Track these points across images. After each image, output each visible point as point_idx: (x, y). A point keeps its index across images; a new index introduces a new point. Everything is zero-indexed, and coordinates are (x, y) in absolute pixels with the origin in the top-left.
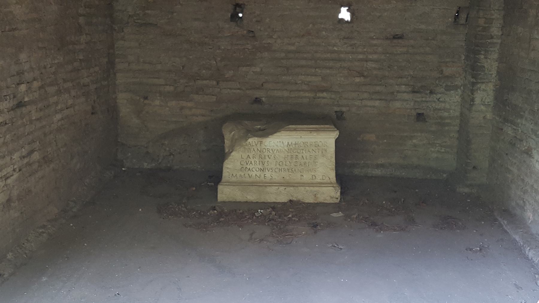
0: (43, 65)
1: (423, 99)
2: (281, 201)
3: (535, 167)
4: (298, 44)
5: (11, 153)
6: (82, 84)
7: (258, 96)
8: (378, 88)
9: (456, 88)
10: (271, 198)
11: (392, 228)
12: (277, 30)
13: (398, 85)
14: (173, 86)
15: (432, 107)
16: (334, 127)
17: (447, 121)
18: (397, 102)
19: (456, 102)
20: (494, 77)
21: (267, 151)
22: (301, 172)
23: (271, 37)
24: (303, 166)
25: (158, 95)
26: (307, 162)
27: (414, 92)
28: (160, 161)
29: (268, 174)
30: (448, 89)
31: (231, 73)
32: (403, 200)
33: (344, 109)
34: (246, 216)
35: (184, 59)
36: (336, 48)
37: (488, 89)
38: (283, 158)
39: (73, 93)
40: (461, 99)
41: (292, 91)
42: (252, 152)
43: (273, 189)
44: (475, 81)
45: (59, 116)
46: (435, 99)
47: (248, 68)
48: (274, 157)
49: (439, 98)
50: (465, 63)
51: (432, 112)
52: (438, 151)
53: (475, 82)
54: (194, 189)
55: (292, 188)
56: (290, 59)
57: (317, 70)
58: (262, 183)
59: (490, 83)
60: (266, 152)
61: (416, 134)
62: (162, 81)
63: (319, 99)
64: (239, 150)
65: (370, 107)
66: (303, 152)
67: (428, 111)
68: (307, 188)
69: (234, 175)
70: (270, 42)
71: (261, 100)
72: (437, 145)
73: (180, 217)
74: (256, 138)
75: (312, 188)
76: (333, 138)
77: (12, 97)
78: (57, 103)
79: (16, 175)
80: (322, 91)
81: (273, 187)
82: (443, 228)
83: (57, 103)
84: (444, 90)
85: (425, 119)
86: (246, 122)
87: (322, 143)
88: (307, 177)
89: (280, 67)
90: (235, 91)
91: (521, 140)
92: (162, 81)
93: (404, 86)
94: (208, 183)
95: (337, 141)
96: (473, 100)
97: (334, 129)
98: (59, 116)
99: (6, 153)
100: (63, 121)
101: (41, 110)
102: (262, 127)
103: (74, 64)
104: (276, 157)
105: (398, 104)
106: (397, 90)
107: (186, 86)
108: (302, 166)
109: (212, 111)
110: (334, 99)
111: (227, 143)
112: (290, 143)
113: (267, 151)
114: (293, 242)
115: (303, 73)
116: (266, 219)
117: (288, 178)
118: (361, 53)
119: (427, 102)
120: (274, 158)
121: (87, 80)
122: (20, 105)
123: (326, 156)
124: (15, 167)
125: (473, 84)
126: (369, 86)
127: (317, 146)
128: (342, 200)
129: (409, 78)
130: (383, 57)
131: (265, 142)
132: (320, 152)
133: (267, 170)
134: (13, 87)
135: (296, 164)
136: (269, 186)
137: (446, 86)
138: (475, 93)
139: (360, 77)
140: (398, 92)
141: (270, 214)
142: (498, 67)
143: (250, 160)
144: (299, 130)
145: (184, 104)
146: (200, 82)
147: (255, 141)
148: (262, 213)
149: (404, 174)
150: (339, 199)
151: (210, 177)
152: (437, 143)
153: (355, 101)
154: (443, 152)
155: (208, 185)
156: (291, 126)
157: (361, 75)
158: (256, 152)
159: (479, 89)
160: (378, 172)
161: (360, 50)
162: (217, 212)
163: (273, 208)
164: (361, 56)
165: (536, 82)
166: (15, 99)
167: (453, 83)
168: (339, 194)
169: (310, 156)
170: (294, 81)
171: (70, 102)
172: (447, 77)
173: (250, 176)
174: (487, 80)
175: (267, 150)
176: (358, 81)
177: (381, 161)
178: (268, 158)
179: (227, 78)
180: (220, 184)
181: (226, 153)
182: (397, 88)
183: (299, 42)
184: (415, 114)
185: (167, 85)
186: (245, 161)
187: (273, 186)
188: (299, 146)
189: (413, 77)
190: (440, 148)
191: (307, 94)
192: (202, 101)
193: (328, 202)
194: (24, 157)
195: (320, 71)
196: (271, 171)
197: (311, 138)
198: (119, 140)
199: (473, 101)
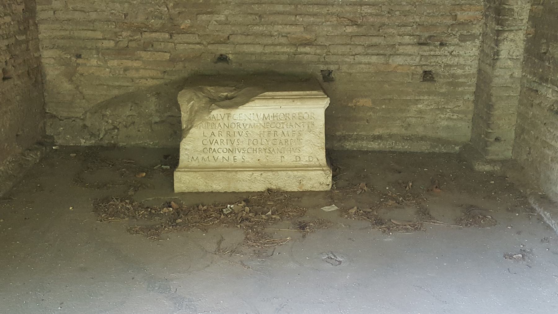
2: (256, 190)
7: (223, 52)
8: (375, 40)
9: (473, 37)
10: (243, 187)
11: (402, 228)
14: (113, 40)
15: (443, 62)
19: (473, 56)
20: (525, 23)
21: (236, 126)
22: (281, 153)
24: (284, 144)
25: (94, 52)
26: (289, 140)
28: (101, 136)
29: (239, 156)
30: (463, 39)
31: (188, 22)
32: (411, 184)
33: (332, 67)
34: (212, 214)
37: (517, 38)
38: (258, 135)
40: (479, 52)
41: (266, 45)
42: (217, 128)
43: (246, 175)
44: (500, 29)
46: (446, 53)
47: (209, 16)
48: (246, 134)
49: (452, 52)
50: (485, 5)
51: (442, 69)
52: (448, 117)
53: (501, 30)
54: (144, 174)
55: (270, 174)
58: (231, 168)
59: (520, 31)
60: (236, 128)
61: (422, 98)
62: (99, 35)
64: (200, 126)
66: (284, 126)
67: (437, 67)
68: (290, 172)
69: (195, 159)
71: (227, 57)
72: (448, 110)
73: (124, 218)
75: (295, 173)
76: (322, 108)
80: (305, 45)
81: (245, 173)
82: (469, 225)
84: (458, 40)
86: (209, 88)
87: (308, 114)
88: (289, 159)
89: (252, 14)
93: (408, 37)
94: (162, 166)
95: (329, 114)
96: (497, 53)
102: (230, 94)
104: (249, 133)
105: (399, 60)
107: (131, 40)
108: (283, 144)
109: (165, 72)
110: (319, 55)
111: (185, 116)
112: (266, 116)
113: (236, 126)
114: (274, 253)
115: (280, 22)
116: (238, 218)
117: (264, 160)
119: (436, 56)
120: (246, 136)
123: (314, 132)
125: (498, 33)
126: (364, 37)
127: (301, 118)
128: (334, 186)
129: (415, 26)
131: (234, 114)
132: (306, 127)
133: (237, 152)
135: (275, 142)
136: (240, 171)
137: (461, 35)
138: (500, 44)
140: (400, 44)
141: (242, 211)
142: (531, 10)
143: (215, 138)
144: (277, 98)
145: (129, 63)
146: (147, 36)
148: (233, 210)
149: (406, 147)
150: (331, 185)
151: (166, 157)
152: (448, 108)
153: (346, 58)
154: (455, 119)
155: (162, 169)
156: (267, 93)
157: (354, 23)
158: (223, 128)
160: (375, 146)
162: (173, 209)
163: (247, 201)
167: (469, 32)
168: (330, 179)
170: (269, 33)
172: (462, 24)
173: (216, 159)
174: (516, 27)
175: (236, 125)
177: (377, 132)
178: (238, 136)
179: (183, 29)
180: (177, 170)
181: (184, 130)
182: (398, 39)
184: (422, 72)
185: (105, 39)
186: (208, 140)
187: (245, 171)
188: (279, 119)
189: (419, 25)
190: (452, 114)
191: (285, 49)
192: (151, 60)
193: (317, 190)
195: (301, 19)
196: (242, 151)
197: (293, 108)
198: (47, 111)
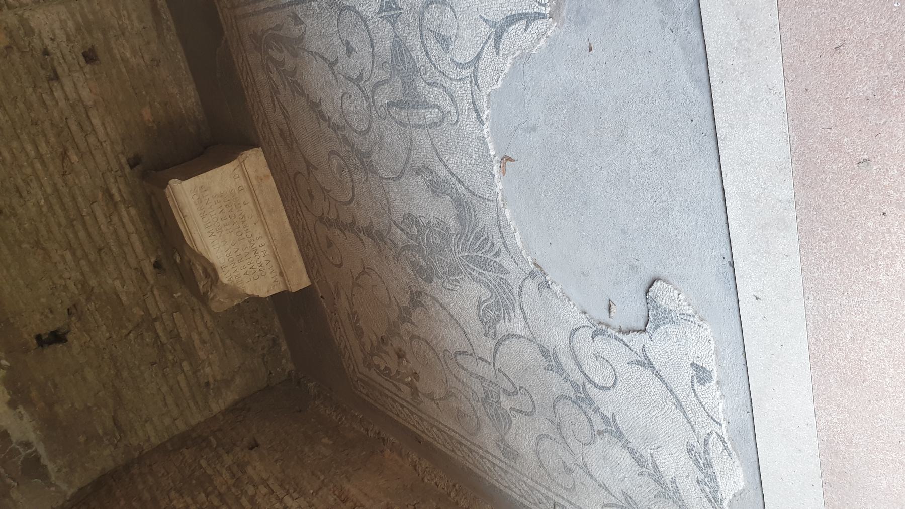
1: (61, 62)
4: (59, 251)
7: (152, 268)
8: (74, 127)
9: (23, 21)
12: (51, 284)
13: (57, 103)
16: (167, 189)
17: (80, 20)
18: (82, 96)
23: (66, 288)
25: (198, 374)
26: (225, 204)
30: (30, 32)
33: (123, 160)
35: (142, 368)
36: (42, 202)
56: (85, 252)
61: (118, 56)
62: (181, 378)
65: (105, 128)
70: (73, 286)
72: (120, 23)
74: (220, 275)
80: (111, 196)
85: (90, 49)
86: (201, 287)
90: (158, 298)
92: (181, 378)
97: (170, 188)
103: (50, 141)
105: (85, 94)
106: (64, 101)
110: (115, 178)
118: (33, 168)
121: (226, 475)
130: (24, 136)
131: (220, 263)
139: (68, 156)
145: (197, 343)
146: (164, 339)
147: (223, 275)
152: (118, 23)
158: (236, 268)
161: (29, 171)
164: (38, 166)
169: (215, 204)
183: (55, 251)
184: (89, 65)
185: (183, 371)
186: (253, 276)
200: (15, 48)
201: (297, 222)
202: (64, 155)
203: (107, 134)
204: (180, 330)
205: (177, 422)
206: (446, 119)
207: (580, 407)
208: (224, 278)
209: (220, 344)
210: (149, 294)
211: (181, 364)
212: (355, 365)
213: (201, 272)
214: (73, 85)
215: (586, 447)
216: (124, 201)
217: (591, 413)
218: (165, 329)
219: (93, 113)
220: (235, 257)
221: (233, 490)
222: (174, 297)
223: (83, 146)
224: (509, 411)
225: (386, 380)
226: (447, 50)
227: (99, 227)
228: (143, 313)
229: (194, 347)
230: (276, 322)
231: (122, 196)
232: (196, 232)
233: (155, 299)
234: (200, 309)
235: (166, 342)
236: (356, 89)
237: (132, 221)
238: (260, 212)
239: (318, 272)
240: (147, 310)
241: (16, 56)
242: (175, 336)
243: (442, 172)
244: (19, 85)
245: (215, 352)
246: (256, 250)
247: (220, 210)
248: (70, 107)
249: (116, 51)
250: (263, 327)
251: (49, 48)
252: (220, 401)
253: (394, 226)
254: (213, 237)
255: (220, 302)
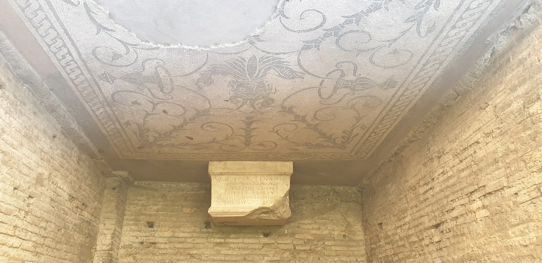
0: (422, 257)
3: (67, 187)
5: (442, 191)
6: (391, 244)
7: (266, 238)
8: (180, 246)
9: (124, 247)
13: (166, 248)
18: (167, 236)
25: (336, 238)
27: (154, 243)
30: (130, 246)
33: (205, 230)
39: (397, 237)
45: (407, 220)
46: (140, 238)
57: (224, 259)
61: (155, 213)
62: (333, 248)
63: (222, 237)
65: (186, 232)
72: (140, 205)
74: (267, 206)
77: (445, 232)
78: (409, 229)
79: (436, 175)
80: (220, 243)
83: (409, 229)
86: (274, 218)
90: (283, 242)
91: (77, 207)
96: (112, 238)
98: (407, 220)
99: (445, 190)
100: (403, 216)
101: (421, 224)
105: (167, 234)
107: (316, 245)
121: (388, 247)
122: (437, 226)
124: (437, 181)
125: (111, 249)
127: (224, 201)
129: (157, 253)
134: (444, 239)
140: (166, 243)
145: (317, 232)
146: (307, 248)
154: (136, 200)
159: (107, 246)
165: (61, 250)
166: (442, 230)
171: (399, 231)
176: (194, 251)
185: (331, 246)
186: (275, 190)
194: (431, 189)
199: (112, 236)
200: (135, 255)
201: (253, 157)
202: (192, 256)
203: (189, 232)
204: (306, 238)
205: (359, 260)
206: (163, 66)
207: (342, 35)
208: (270, 205)
209: (324, 221)
210: (280, 245)
211: (326, 245)
212: (347, 154)
213: (265, 215)
214: (161, 238)
215: (372, 37)
216: (225, 238)
217: (344, 30)
218: (302, 245)
219: (176, 235)
220: (261, 195)
221: (394, 247)
222: (287, 234)
223: (190, 246)
224: (356, 78)
225: (352, 140)
226: (121, 56)
227: (233, 255)
228: (289, 253)
229: (320, 235)
230: (325, 187)
231: (222, 238)
232: (238, 210)
233: (283, 244)
234: (299, 223)
235: (310, 248)
236: (159, 106)
237: (237, 238)
238: (243, 174)
239: (283, 156)
240: (287, 250)
241: (138, 257)
242: (307, 242)
243: (196, 76)
244: (151, 261)
245: (327, 225)
246: (262, 183)
247: (233, 193)
248: (170, 244)
249: (152, 213)
250: (324, 195)
251: (140, 241)
252: (358, 234)
253: (240, 109)
254: (246, 202)
255: (285, 212)
